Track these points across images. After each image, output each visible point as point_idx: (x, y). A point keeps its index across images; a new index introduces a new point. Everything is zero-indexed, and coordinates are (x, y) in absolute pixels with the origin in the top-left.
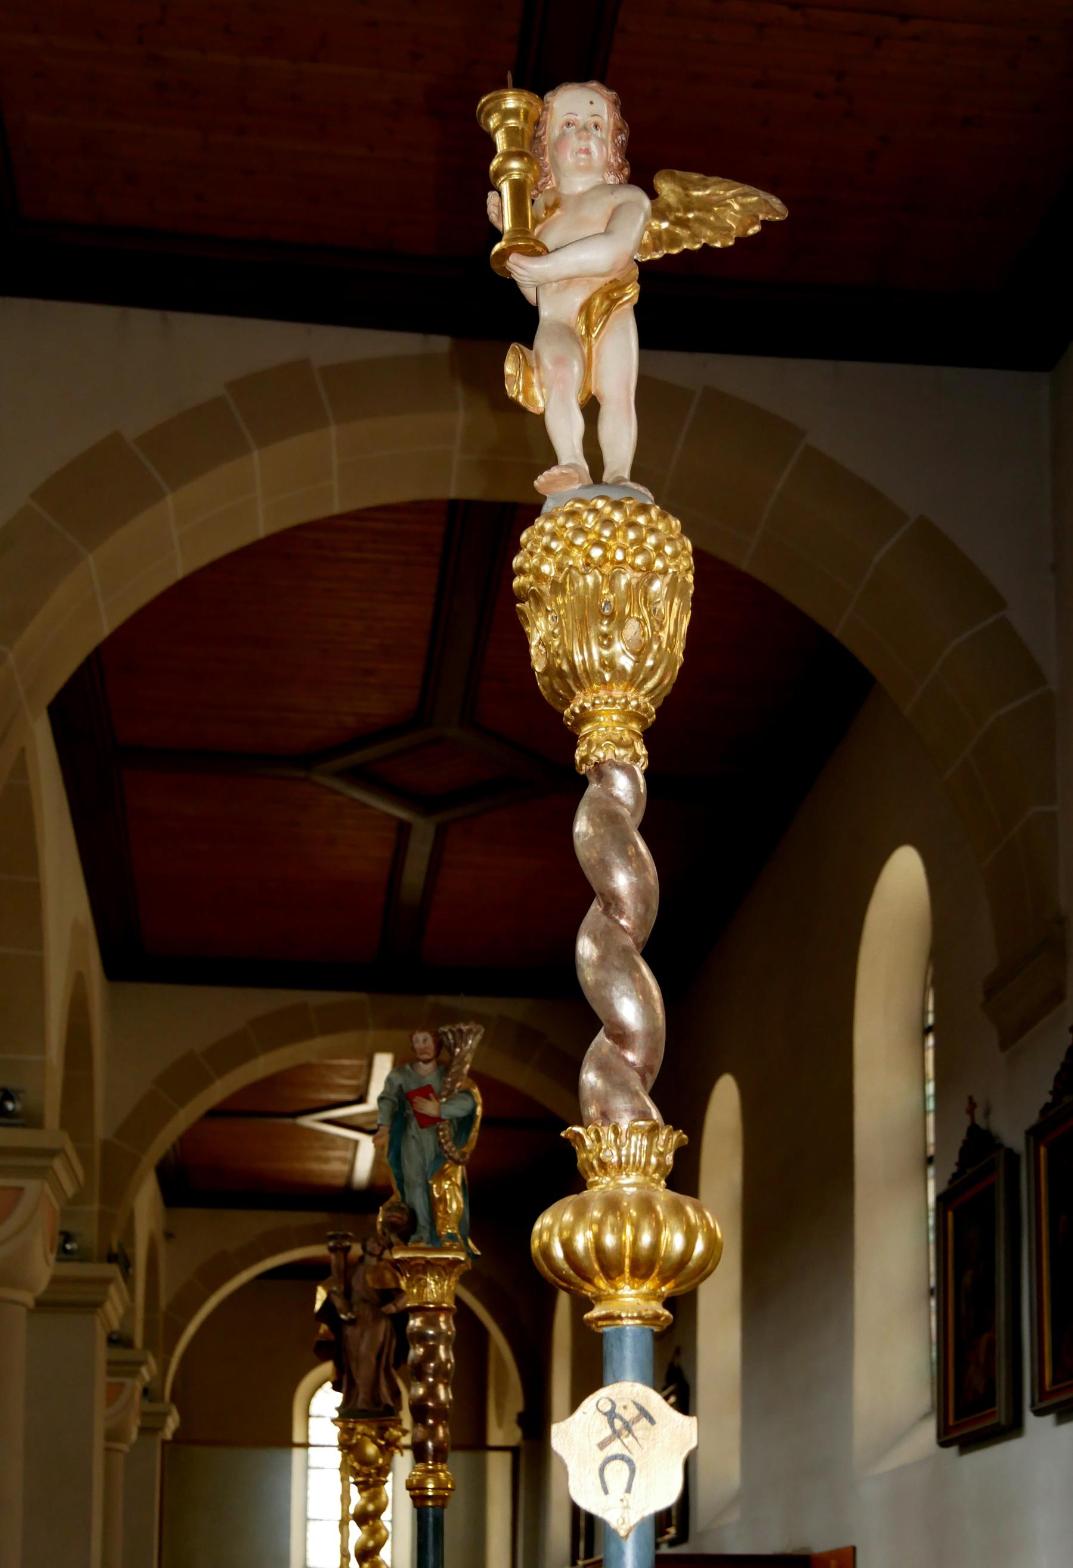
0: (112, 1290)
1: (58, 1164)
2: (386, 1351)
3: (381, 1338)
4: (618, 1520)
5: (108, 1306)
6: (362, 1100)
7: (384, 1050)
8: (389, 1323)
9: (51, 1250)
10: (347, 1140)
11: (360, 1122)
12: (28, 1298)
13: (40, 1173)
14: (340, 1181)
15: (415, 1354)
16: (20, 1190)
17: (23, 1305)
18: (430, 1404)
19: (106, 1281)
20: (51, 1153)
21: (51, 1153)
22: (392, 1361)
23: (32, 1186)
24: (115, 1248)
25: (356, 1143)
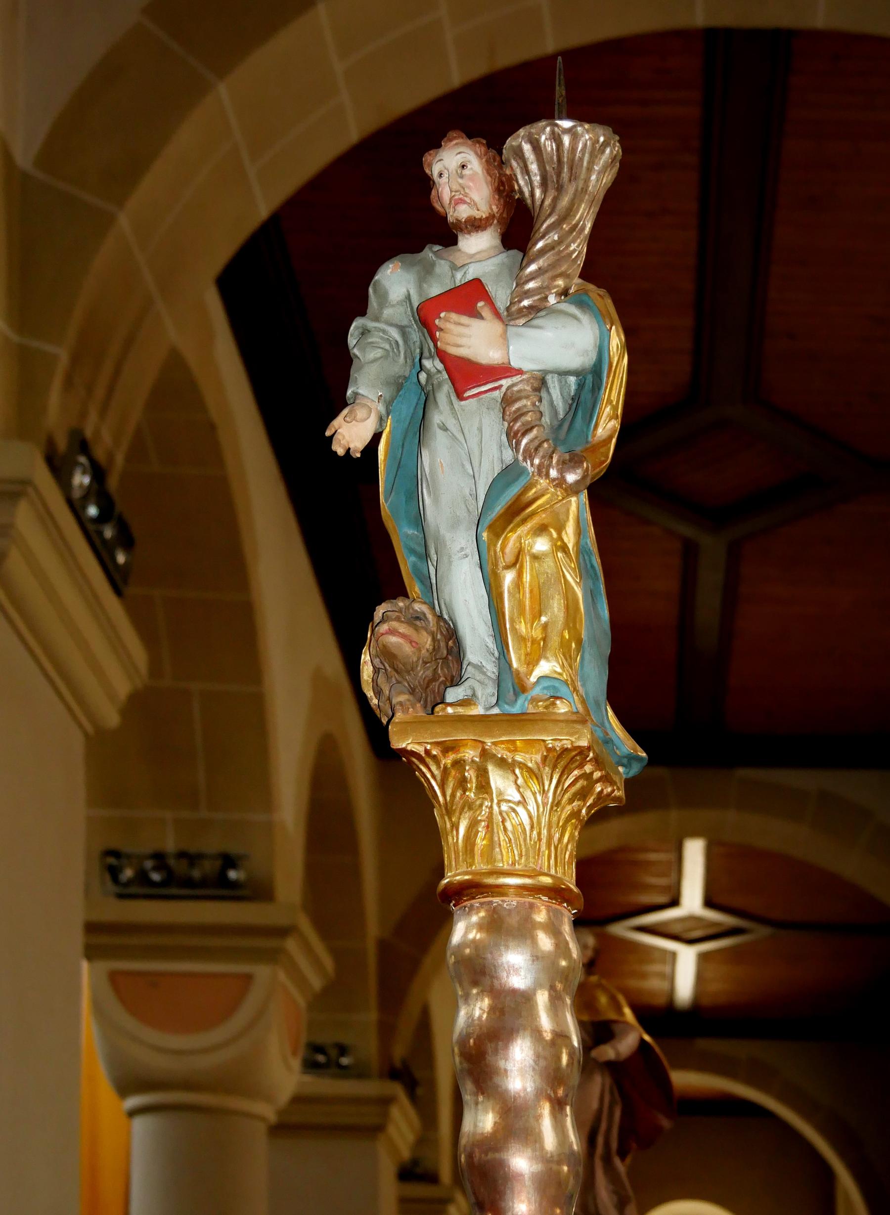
0: (395, 1112)
1: (291, 945)
2: (603, 1126)
3: (595, 1105)
4: (457, 172)
5: (391, 1130)
6: (675, 902)
7: (694, 834)
8: (608, 1081)
9: (294, 1053)
10: (664, 952)
11: (677, 929)
12: (268, 1112)
13: (272, 956)
14: (661, 1001)
15: (470, 1016)
16: (248, 979)
17: (262, 1119)
18: (565, 1168)
19: (386, 1102)
20: (283, 932)
21: (283, 932)
22: (614, 1145)
23: (262, 972)
24: (398, 1063)
25: (674, 955)
